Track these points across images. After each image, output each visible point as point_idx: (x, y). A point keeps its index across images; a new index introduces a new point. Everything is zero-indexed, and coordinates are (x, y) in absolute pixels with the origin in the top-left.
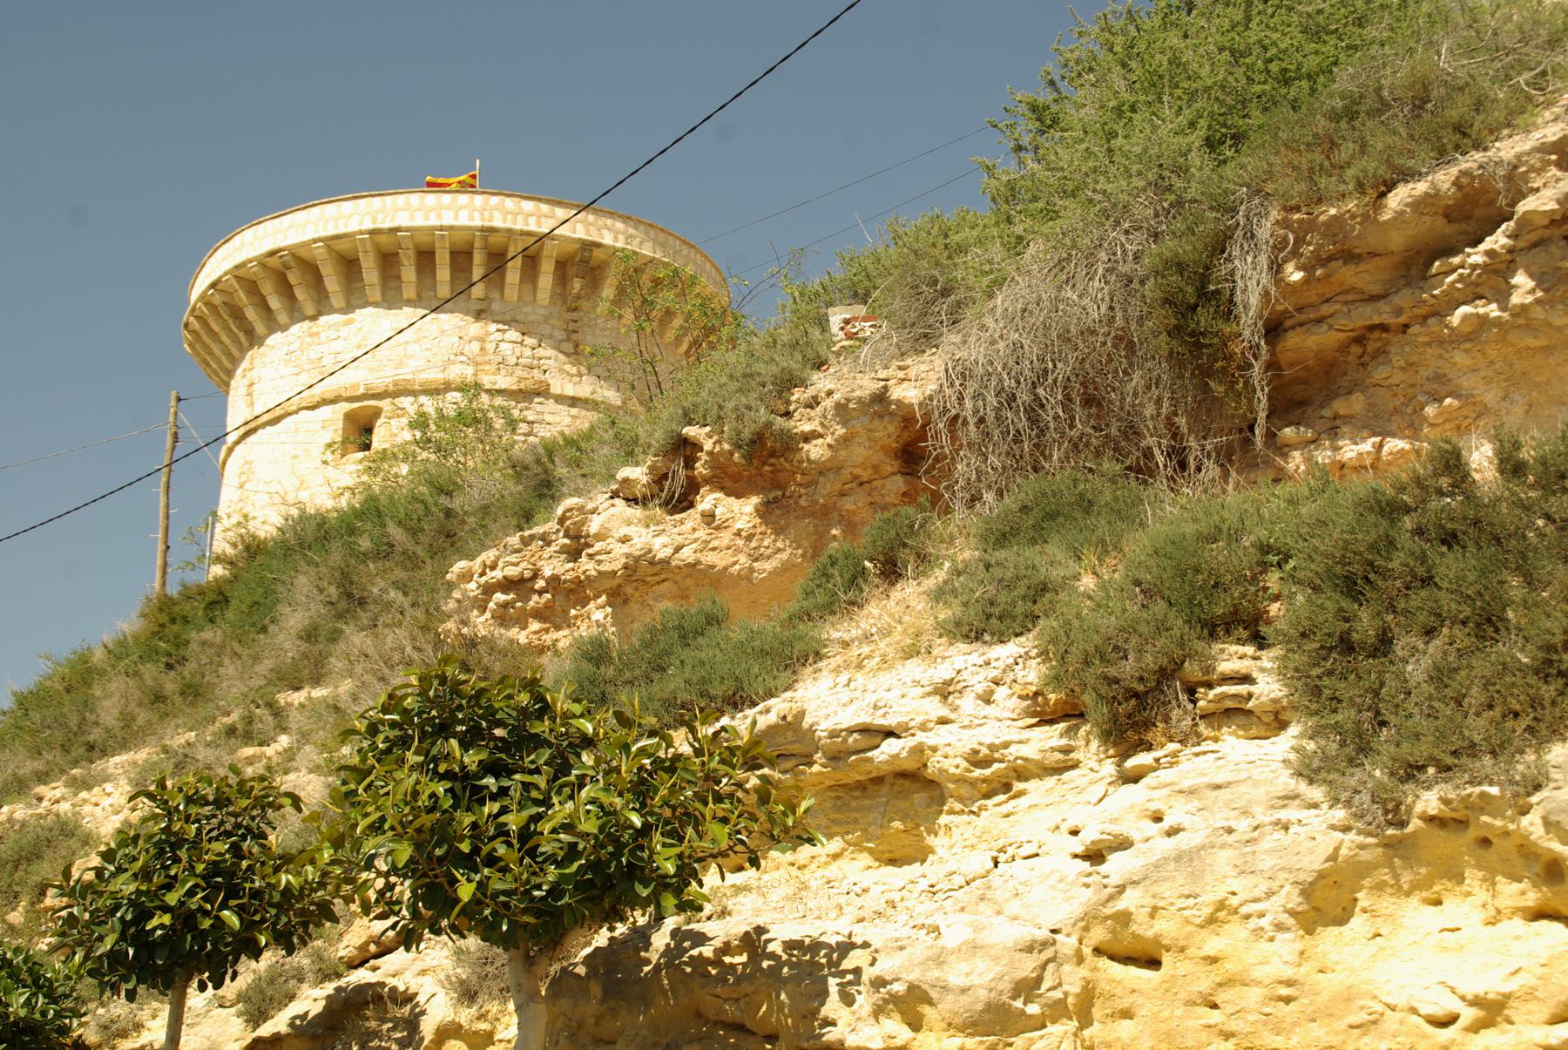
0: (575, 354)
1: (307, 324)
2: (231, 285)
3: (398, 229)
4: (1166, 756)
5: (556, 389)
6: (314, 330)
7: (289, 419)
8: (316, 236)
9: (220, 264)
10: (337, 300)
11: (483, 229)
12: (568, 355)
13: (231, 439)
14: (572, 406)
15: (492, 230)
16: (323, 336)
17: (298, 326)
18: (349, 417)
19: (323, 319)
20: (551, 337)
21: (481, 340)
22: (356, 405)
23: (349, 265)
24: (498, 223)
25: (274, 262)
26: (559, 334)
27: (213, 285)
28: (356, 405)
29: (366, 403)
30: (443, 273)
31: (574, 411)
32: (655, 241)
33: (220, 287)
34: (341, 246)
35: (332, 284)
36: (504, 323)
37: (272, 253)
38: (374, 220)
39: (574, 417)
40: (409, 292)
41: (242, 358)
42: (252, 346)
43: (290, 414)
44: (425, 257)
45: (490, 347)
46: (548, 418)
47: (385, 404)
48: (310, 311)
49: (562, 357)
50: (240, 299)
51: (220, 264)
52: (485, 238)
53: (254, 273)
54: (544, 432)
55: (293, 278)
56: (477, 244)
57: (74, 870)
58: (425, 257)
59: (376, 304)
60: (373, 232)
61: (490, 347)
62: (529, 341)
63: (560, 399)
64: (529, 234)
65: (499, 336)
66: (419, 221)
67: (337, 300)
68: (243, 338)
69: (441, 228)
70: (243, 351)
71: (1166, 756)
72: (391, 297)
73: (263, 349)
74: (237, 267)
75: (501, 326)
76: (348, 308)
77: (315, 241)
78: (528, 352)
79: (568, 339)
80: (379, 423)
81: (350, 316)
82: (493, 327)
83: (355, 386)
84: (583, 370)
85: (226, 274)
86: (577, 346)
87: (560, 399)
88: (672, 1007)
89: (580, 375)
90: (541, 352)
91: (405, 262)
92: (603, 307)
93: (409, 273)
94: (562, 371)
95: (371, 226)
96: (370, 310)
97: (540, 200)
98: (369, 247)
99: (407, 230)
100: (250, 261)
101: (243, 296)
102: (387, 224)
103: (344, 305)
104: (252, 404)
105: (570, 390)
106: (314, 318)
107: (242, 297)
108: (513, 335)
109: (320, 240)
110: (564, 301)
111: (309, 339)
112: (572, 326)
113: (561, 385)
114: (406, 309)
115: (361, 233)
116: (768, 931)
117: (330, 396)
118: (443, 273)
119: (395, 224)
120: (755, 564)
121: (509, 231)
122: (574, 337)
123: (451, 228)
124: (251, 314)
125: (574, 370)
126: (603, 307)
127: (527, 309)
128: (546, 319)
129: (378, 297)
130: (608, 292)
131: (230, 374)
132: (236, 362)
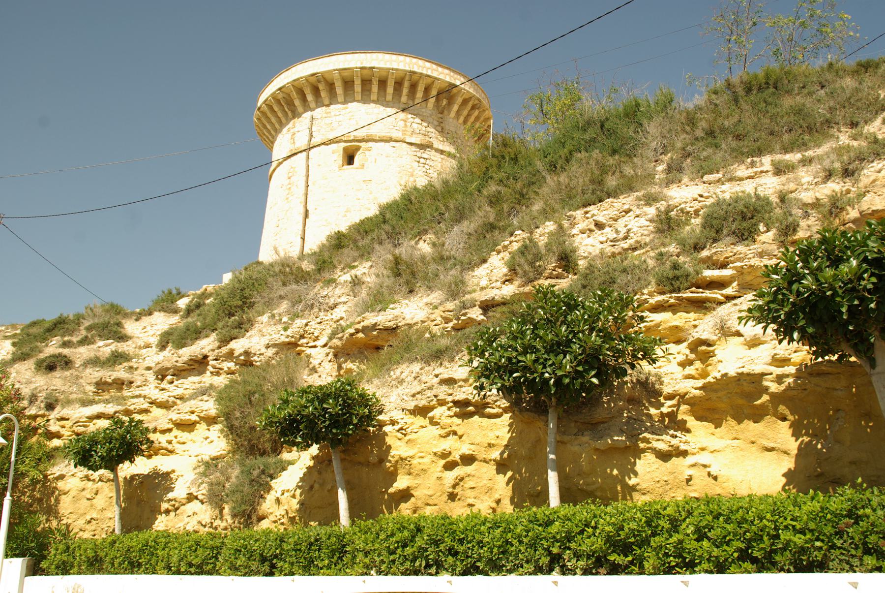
0: (442, 131)
1: (324, 108)
2: (290, 89)
3: (373, 68)
5: (435, 146)
6: (328, 111)
7: (315, 149)
8: (335, 68)
10: (340, 98)
11: (410, 72)
12: (439, 132)
13: (274, 165)
14: (441, 154)
15: (414, 73)
16: (333, 114)
17: (320, 109)
18: (345, 150)
19: (332, 107)
20: (432, 123)
21: (405, 121)
22: (349, 144)
23: (348, 84)
24: (416, 69)
25: (313, 79)
26: (436, 123)
28: (349, 144)
29: (353, 144)
30: (390, 90)
31: (442, 156)
32: (474, 89)
33: (283, 90)
34: (346, 74)
35: (339, 90)
36: (414, 115)
37: (313, 75)
38: (362, 63)
39: (442, 159)
40: (374, 96)
41: (288, 123)
42: (294, 117)
44: (383, 83)
45: (408, 124)
46: (433, 158)
47: (362, 144)
48: (327, 102)
49: (437, 132)
50: (293, 95)
52: (411, 76)
54: (34, 408)
55: (321, 87)
56: (407, 78)
58: (383, 83)
59: (358, 101)
60: (362, 68)
61: (408, 124)
62: (425, 124)
63: (437, 150)
64: (429, 76)
65: (412, 120)
66: (382, 65)
67: (340, 98)
68: (290, 114)
69: (393, 69)
70: (288, 120)
73: (300, 119)
74: (294, 80)
75: (413, 116)
76: (345, 102)
77: (334, 70)
78: (424, 129)
79: (439, 126)
82: (410, 116)
84: (445, 140)
85: (288, 83)
86: (442, 129)
87: (437, 150)
88: (642, 410)
89: (444, 142)
90: (429, 129)
91: (375, 83)
92: (453, 114)
93: (375, 88)
94: (437, 138)
95: (362, 66)
96: (355, 104)
97: (433, 63)
98: (359, 75)
99: (377, 68)
100: (301, 78)
102: (368, 65)
104: (294, 143)
105: (441, 147)
106: (328, 106)
107: (294, 94)
108: (418, 120)
109: (337, 70)
110: (438, 109)
111: (325, 115)
112: (440, 120)
113: (437, 145)
114: (372, 104)
115: (356, 68)
116: (153, 451)
118: (390, 90)
121: (421, 74)
122: (442, 125)
123: (397, 70)
124: (297, 102)
125: (441, 139)
126: (453, 114)
127: (424, 110)
128: (431, 115)
129: (360, 98)
130: (455, 108)
131: (273, 143)
132: (282, 125)
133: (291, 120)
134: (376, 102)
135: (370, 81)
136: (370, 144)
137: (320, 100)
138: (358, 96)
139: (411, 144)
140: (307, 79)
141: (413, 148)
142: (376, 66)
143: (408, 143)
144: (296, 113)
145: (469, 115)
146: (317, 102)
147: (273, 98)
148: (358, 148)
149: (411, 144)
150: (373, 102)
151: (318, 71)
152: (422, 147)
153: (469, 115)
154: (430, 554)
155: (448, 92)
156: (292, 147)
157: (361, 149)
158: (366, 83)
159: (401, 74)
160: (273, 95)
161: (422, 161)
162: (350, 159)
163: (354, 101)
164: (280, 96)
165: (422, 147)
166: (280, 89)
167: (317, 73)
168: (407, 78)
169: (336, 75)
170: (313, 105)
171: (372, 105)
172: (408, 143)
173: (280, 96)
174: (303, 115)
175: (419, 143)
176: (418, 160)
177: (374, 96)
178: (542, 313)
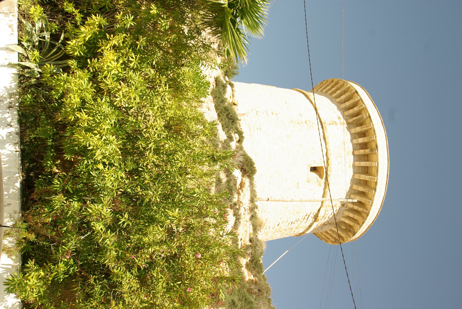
2: (369, 126)
3: (375, 191)
4: (34, 275)
8: (379, 164)
9: (363, 94)
10: (357, 164)
15: (367, 215)
19: (352, 156)
20: (331, 220)
24: (369, 217)
26: (330, 222)
27: (356, 92)
29: (325, 174)
33: (368, 118)
40: (355, 187)
42: (348, 123)
43: (326, 144)
47: (323, 180)
48: (356, 153)
50: (364, 128)
51: (363, 94)
52: (365, 213)
53: (371, 137)
56: (365, 211)
57: (97, 60)
59: (353, 176)
64: (363, 223)
67: (357, 164)
68: (351, 120)
69: (372, 203)
71: (34, 275)
72: (355, 181)
73: (346, 129)
74: (374, 131)
76: (354, 166)
77: (378, 163)
78: (328, 216)
80: (318, 177)
81: (352, 167)
83: (331, 171)
91: (364, 189)
95: (378, 183)
100: (376, 137)
101: (365, 129)
103: (355, 165)
106: (353, 153)
107: (364, 128)
109: (378, 165)
117: (329, 162)
119: (377, 190)
120: (107, 163)
121: (366, 219)
133: (346, 120)
134: (351, 188)
135: (368, 161)
136: (323, 185)
137: (357, 136)
138: (357, 176)
139: (319, 210)
140: (375, 141)
141: (316, 211)
142: (376, 193)
143: (320, 209)
144: (351, 126)
145: (331, 236)
146: (355, 134)
147: (363, 108)
148: (321, 176)
149: (319, 210)
150: (352, 186)
151: (379, 151)
152: (316, 218)
153: (331, 236)
154: (91, 208)
155: (350, 230)
156: (327, 122)
157: (320, 179)
158: (366, 171)
159: (368, 207)
160: (365, 109)
161: (306, 217)
162: (314, 169)
163: (354, 173)
164: (364, 116)
165: (316, 218)
166: (369, 117)
167: (377, 149)
168: (365, 211)
169: (374, 164)
170: (355, 141)
171: (349, 185)
172: (320, 209)
173: (364, 116)
174: (348, 132)
175: (319, 216)
176: (308, 215)
177: (355, 187)
178: (57, 163)
